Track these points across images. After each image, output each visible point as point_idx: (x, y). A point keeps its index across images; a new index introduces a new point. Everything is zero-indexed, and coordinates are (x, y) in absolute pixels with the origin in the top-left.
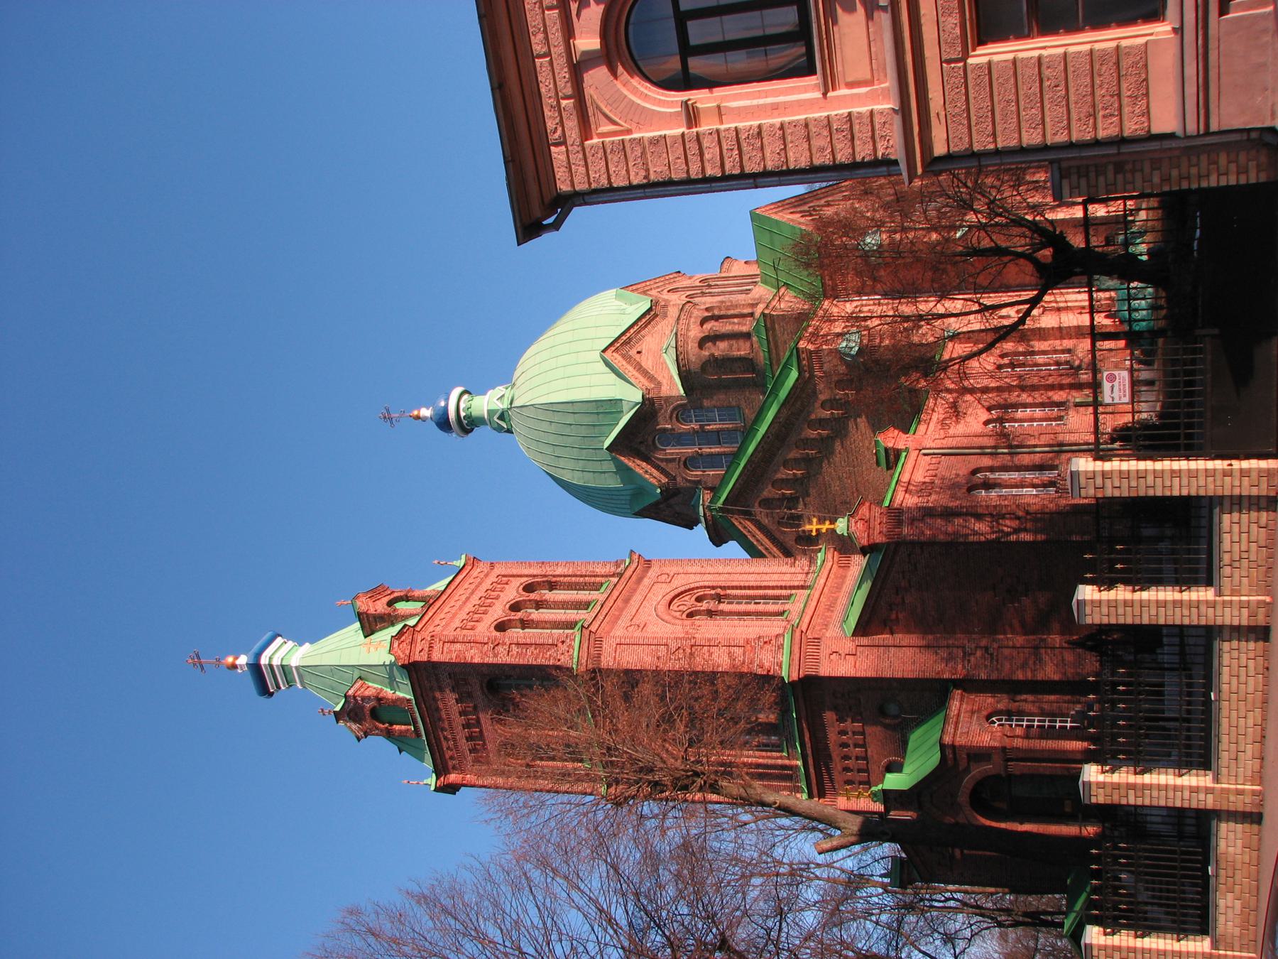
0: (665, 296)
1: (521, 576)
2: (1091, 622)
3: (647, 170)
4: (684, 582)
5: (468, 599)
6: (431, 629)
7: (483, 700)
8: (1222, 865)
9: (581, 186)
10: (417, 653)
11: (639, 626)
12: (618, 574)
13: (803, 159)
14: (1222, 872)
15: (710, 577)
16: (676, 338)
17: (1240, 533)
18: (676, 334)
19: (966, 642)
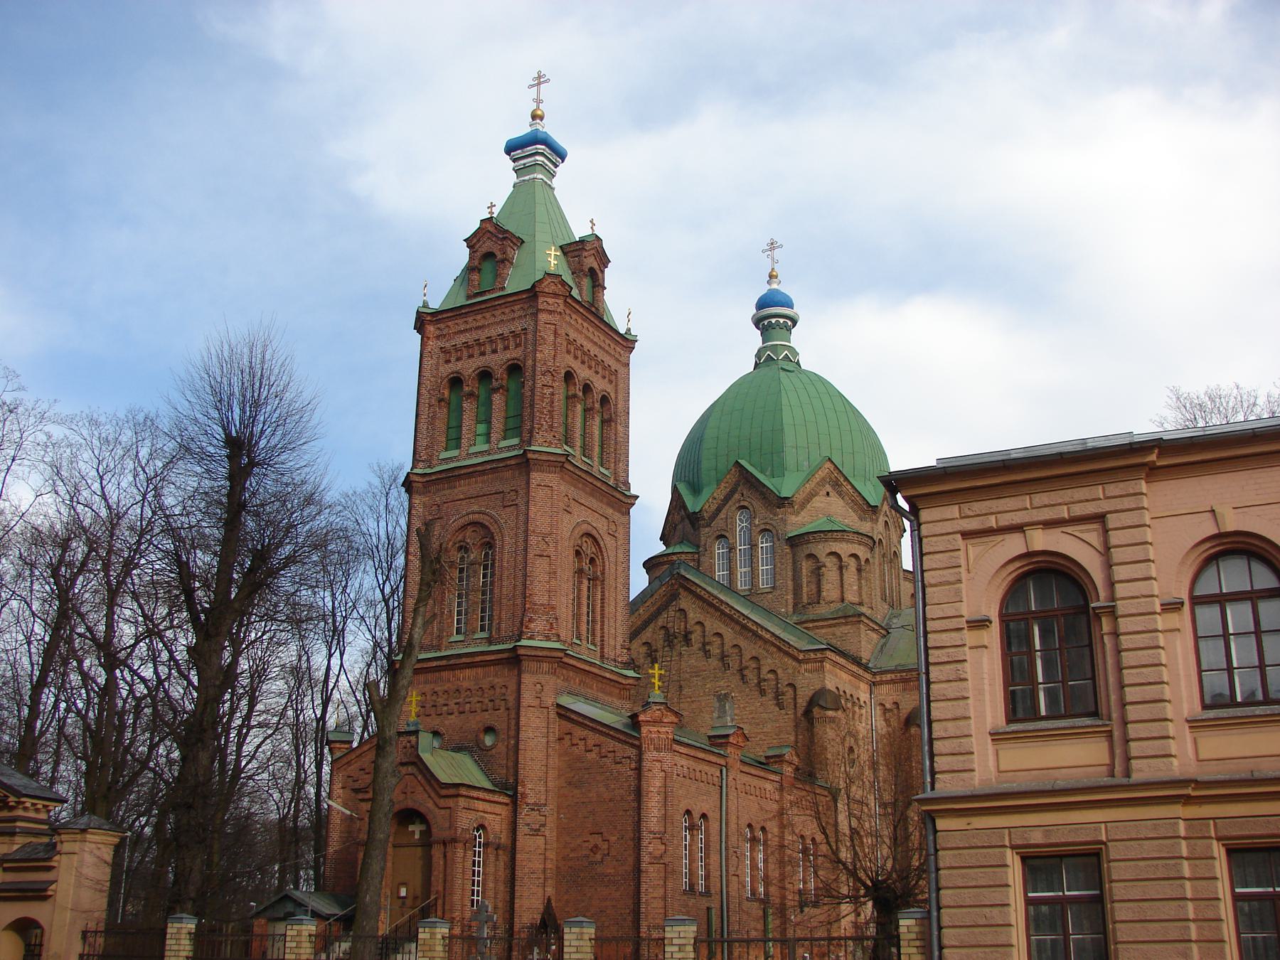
0: (882, 519)
1: (616, 392)
2: (565, 931)
5: (595, 343)
7: (502, 360)
9: (925, 530)
10: (546, 299)
13: (938, 714)
15: (613, 571)
16: (840, 531)
18: (844, 531)
19: (551, 807)
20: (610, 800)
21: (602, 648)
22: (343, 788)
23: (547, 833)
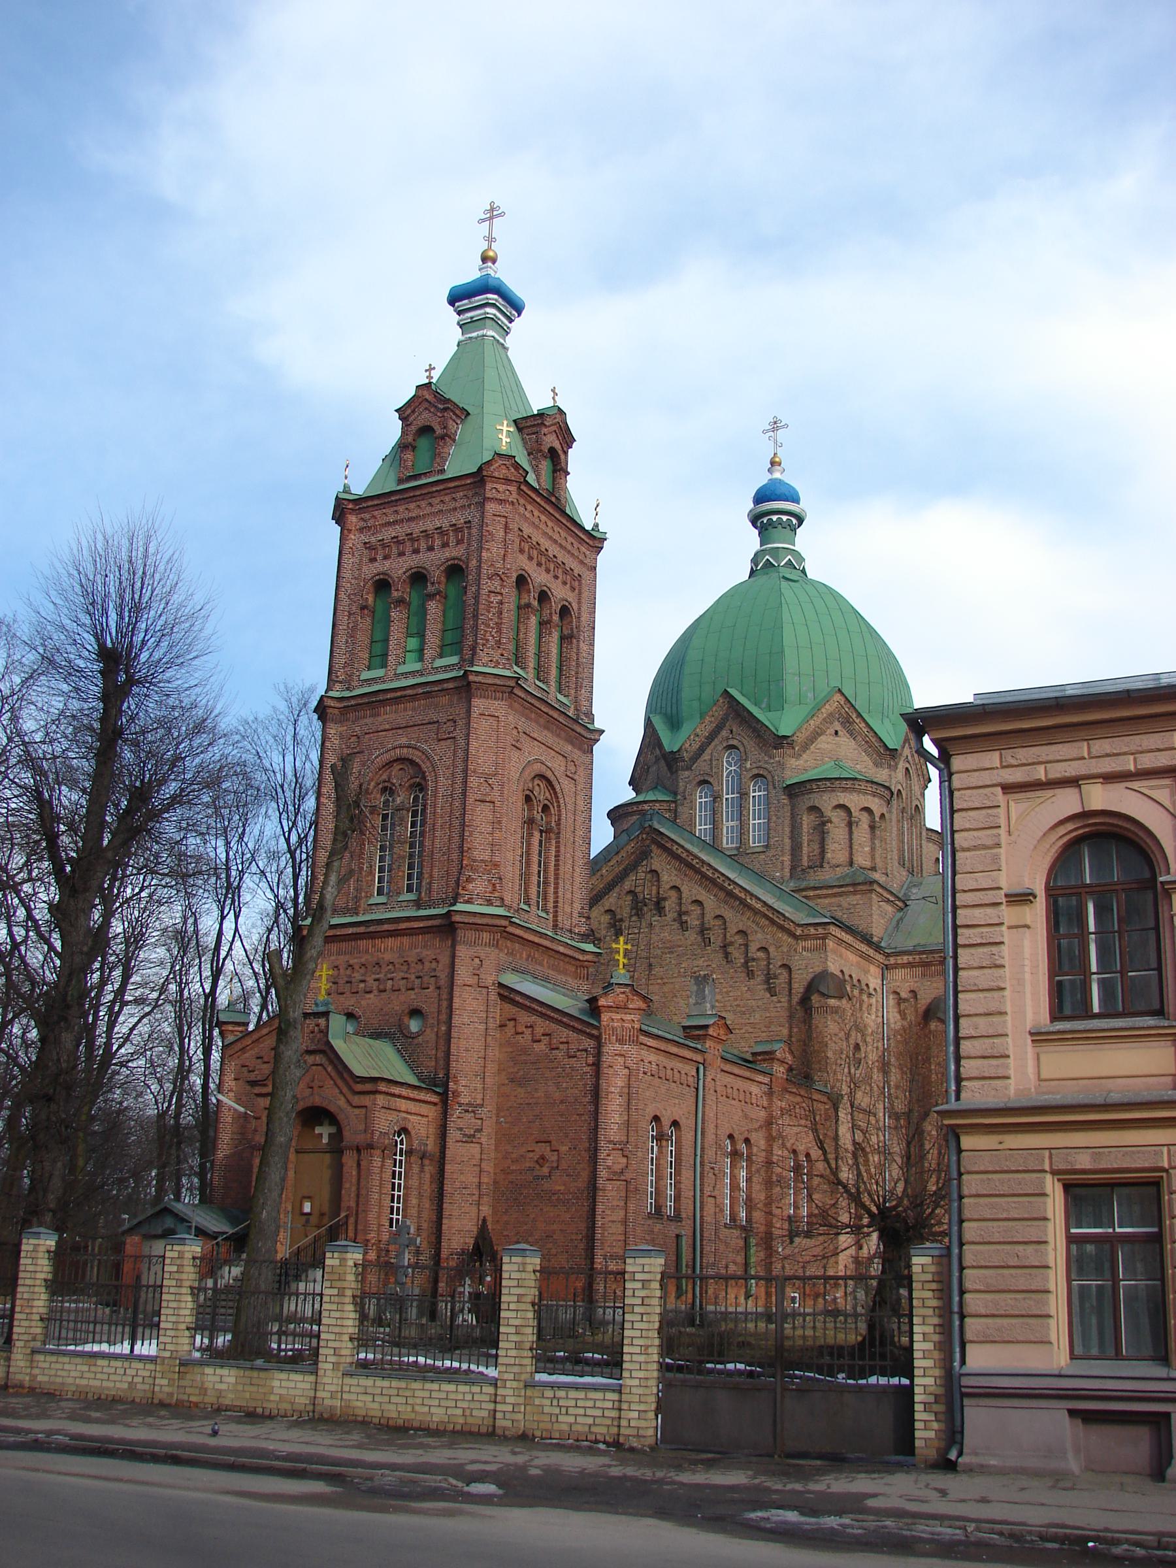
0: (902, 765)
1: (579, 603)
3: (968, 850)
4: (566, 791)
5: (555, 541)
6: (522, 501)
8: (263, 1374)
11: (518, 741)
12: (578, 715)
14: (255, 1374)
15: (571, 821)
16: (850, 779)
17: (585, 1408)
18: (855, 779)
20: (562, 1102)
21: (555, 916)
22: (235, 1079)
23: (484, 1140)
